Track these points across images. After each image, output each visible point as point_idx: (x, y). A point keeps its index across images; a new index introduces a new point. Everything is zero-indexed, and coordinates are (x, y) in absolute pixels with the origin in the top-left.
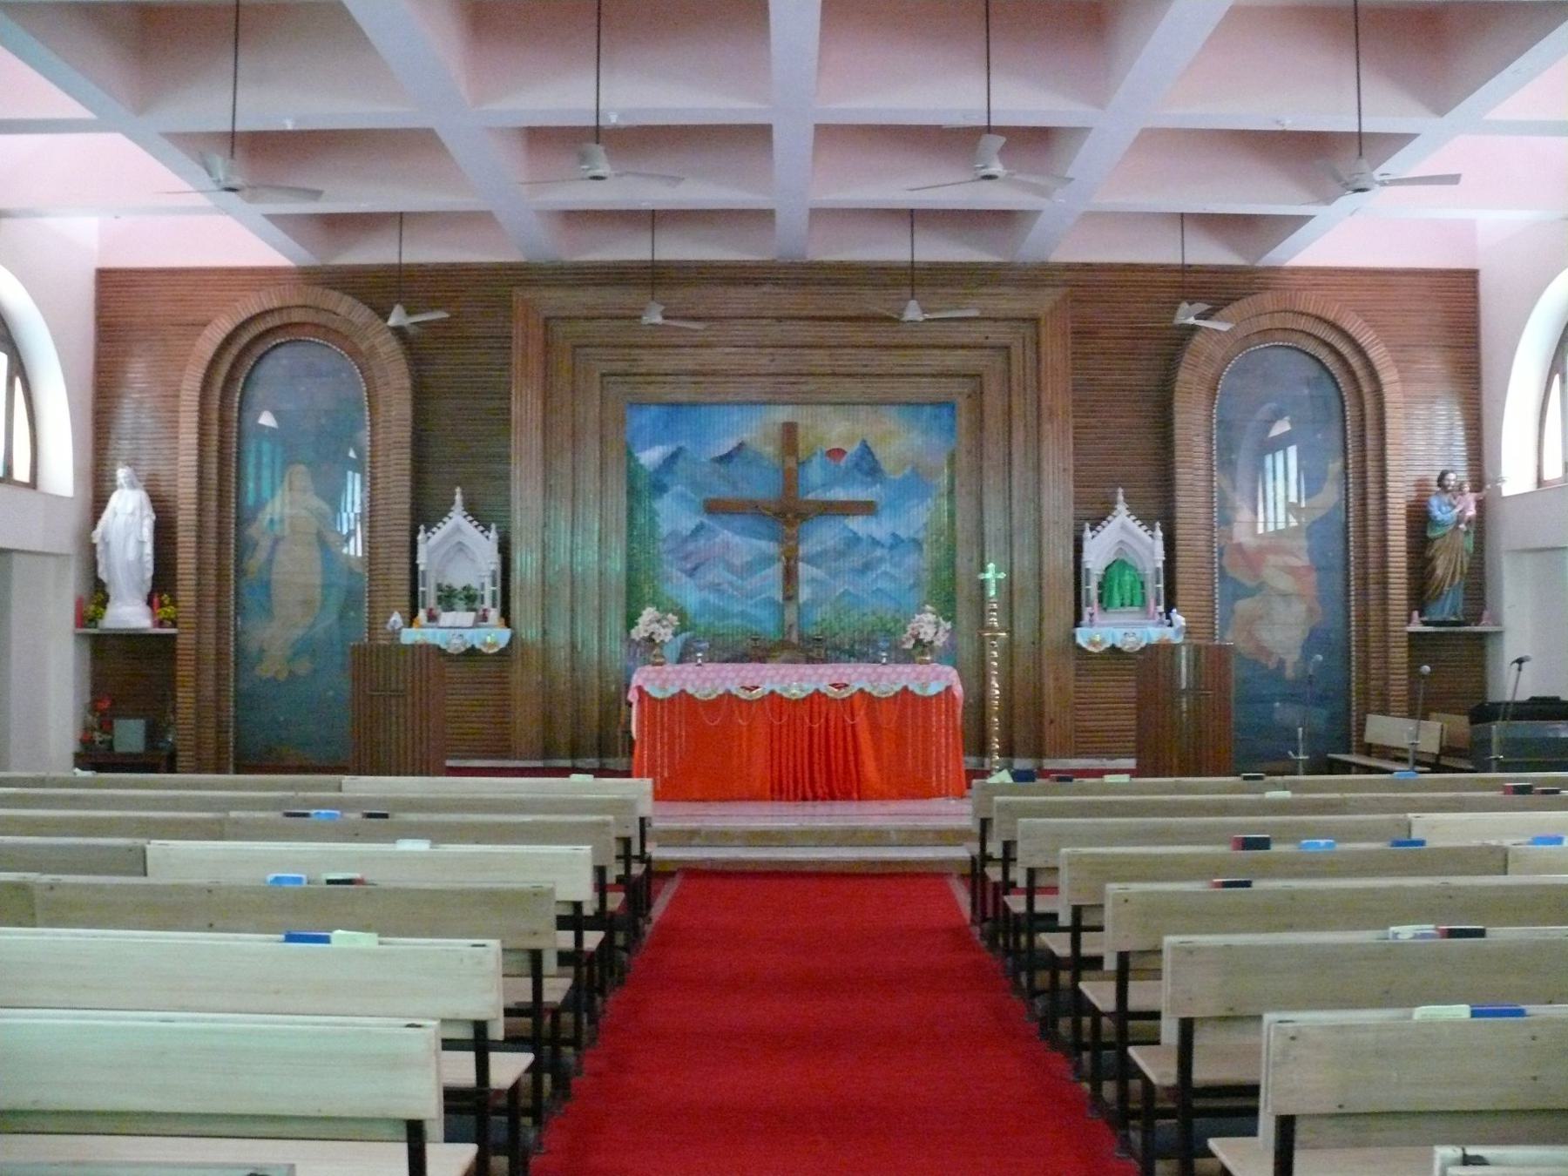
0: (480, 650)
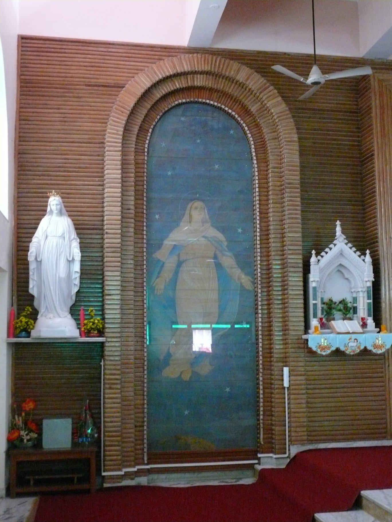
0: (370, 351)
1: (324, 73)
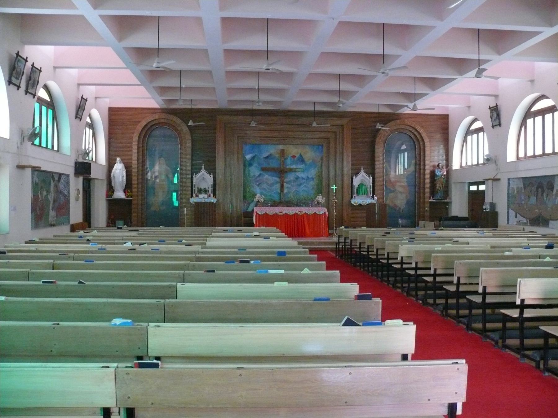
1: (194, 123)
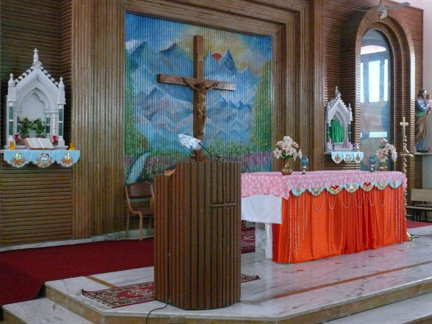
0: (60, 165)
